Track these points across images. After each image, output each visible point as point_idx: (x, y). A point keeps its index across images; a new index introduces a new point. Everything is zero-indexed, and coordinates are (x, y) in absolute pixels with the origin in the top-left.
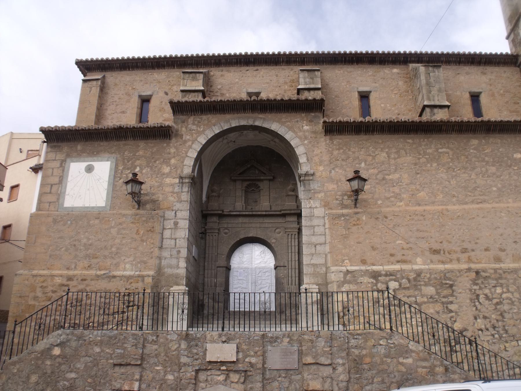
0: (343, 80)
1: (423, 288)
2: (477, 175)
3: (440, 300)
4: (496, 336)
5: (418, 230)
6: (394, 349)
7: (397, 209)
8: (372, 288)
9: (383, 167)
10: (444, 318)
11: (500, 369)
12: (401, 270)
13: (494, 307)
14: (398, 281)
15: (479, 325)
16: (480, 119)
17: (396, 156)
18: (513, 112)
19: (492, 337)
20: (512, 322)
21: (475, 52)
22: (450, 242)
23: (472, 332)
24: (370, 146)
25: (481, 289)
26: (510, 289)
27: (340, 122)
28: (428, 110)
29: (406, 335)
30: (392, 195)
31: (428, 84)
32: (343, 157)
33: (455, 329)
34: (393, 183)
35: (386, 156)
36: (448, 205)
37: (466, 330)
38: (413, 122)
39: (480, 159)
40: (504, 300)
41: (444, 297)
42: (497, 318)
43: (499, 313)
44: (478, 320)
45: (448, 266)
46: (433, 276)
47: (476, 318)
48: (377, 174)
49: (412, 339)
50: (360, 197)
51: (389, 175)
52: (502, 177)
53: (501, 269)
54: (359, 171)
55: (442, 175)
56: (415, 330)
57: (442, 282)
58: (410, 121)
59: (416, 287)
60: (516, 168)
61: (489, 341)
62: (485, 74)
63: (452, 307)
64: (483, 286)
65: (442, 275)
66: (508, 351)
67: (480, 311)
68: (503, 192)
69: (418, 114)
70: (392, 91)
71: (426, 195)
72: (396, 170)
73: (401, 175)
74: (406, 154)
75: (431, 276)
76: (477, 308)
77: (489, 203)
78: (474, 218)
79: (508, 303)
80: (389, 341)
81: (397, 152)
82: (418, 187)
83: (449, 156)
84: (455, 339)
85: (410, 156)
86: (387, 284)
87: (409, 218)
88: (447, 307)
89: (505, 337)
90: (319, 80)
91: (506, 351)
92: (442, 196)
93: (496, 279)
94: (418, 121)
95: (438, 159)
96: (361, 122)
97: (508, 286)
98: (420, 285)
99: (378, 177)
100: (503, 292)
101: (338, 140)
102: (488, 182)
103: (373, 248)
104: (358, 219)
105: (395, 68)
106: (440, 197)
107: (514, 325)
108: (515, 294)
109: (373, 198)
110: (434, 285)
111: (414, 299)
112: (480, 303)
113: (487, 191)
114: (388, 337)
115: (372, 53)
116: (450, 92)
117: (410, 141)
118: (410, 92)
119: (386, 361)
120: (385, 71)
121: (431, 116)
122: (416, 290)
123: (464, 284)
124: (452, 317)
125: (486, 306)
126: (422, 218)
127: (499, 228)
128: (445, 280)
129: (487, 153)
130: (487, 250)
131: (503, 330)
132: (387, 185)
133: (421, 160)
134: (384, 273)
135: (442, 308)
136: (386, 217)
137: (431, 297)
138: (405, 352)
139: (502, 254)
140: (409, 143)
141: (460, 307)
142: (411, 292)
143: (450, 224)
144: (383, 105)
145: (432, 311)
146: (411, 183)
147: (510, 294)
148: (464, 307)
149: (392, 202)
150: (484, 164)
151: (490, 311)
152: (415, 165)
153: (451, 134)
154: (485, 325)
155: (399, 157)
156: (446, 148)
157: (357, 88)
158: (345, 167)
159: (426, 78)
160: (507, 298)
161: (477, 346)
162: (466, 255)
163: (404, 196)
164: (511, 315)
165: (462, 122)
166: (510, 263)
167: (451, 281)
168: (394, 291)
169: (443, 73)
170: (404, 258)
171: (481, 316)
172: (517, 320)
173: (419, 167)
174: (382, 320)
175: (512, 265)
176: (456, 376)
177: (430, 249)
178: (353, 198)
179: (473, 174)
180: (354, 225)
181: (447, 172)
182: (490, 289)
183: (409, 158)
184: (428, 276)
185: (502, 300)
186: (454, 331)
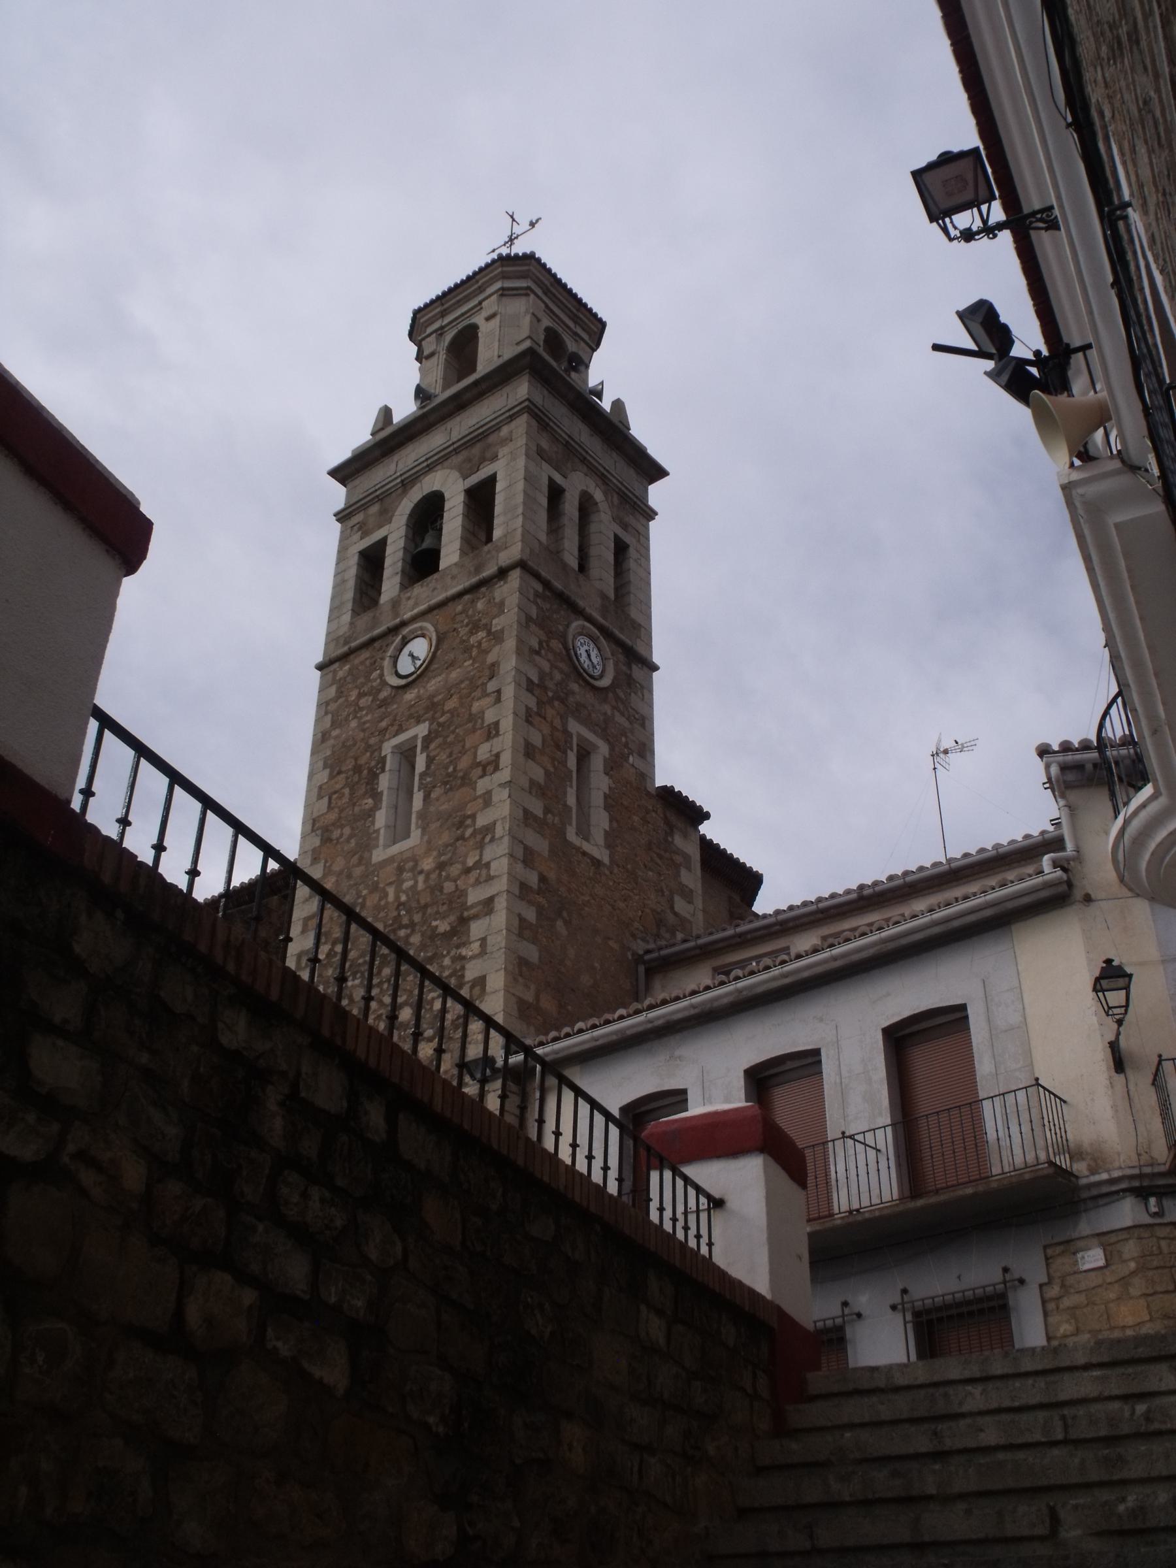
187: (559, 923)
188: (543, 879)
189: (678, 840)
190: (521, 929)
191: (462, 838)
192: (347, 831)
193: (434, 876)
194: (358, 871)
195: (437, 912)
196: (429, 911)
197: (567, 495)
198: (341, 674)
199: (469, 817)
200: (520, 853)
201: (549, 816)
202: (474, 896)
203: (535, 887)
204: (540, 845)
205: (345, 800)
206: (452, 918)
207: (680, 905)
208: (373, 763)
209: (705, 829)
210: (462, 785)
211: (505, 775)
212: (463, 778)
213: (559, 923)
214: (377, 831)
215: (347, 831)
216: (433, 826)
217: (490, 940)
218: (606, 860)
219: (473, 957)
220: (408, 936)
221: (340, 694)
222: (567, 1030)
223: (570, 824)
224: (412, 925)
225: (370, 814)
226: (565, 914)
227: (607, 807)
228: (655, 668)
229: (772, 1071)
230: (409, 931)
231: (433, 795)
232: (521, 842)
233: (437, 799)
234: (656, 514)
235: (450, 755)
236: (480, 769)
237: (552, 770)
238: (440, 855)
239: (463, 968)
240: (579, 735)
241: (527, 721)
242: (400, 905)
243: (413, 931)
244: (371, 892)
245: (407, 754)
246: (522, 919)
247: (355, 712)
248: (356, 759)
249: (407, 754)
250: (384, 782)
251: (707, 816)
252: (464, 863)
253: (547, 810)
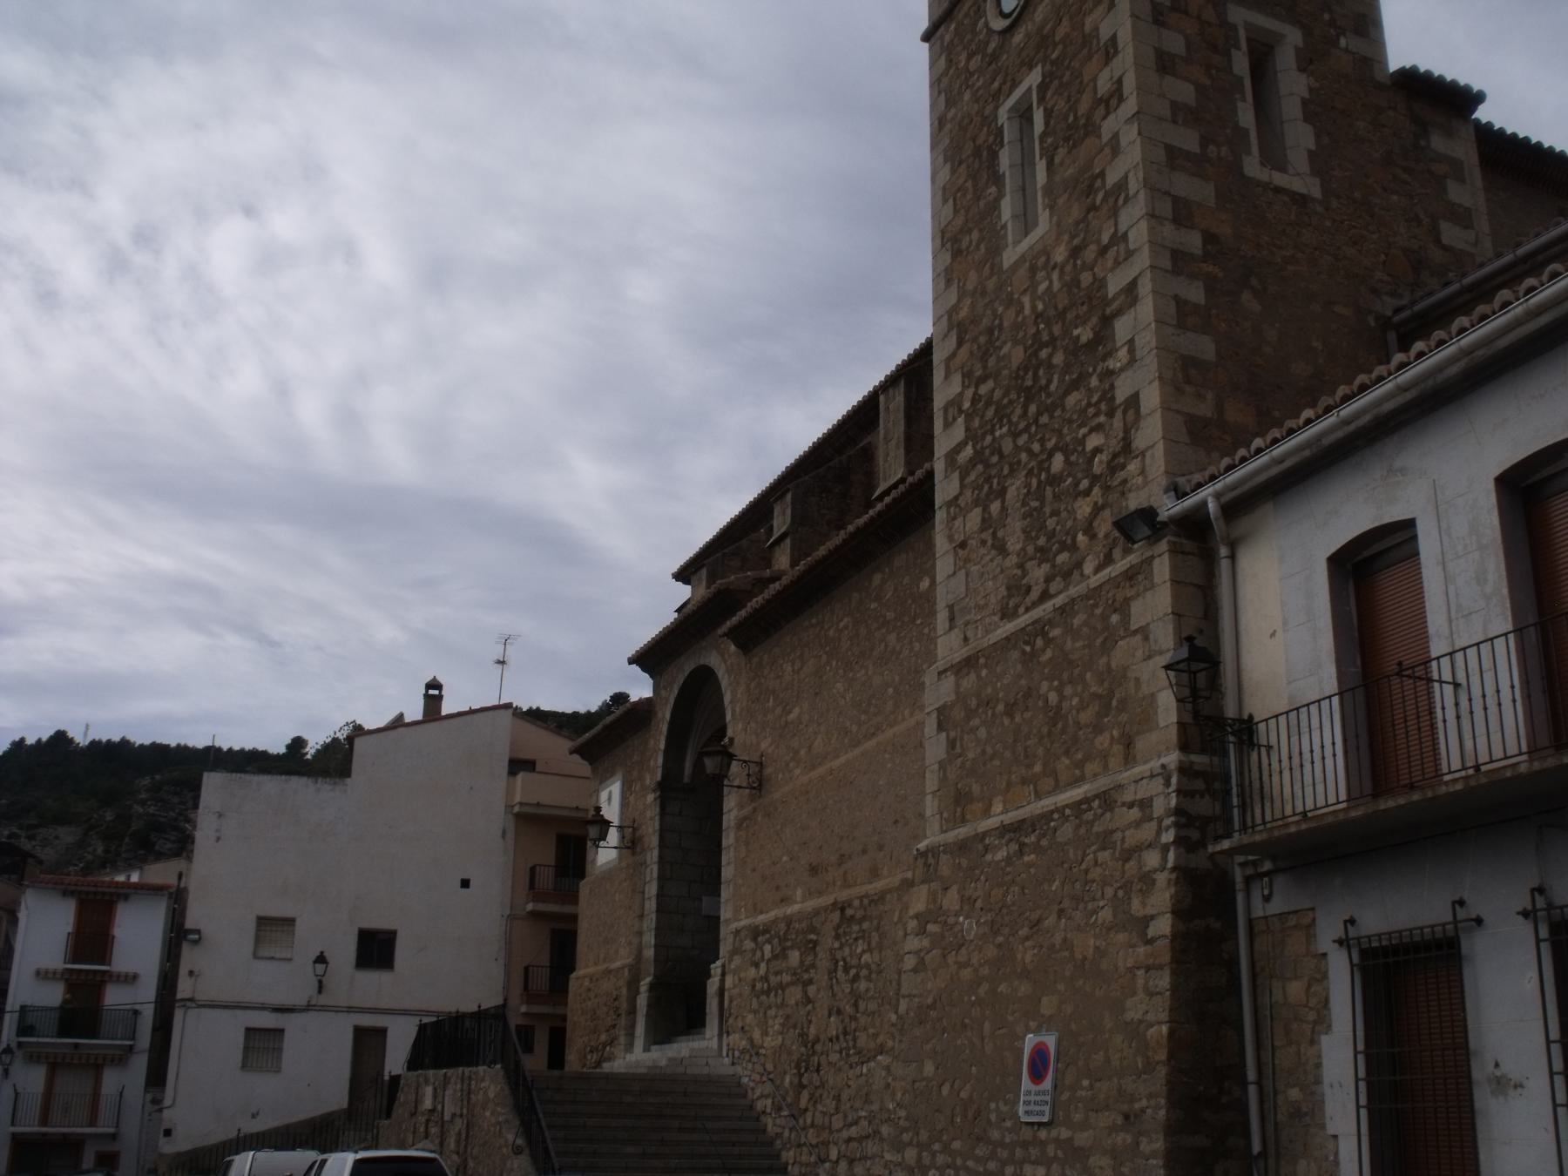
187: (1246, 296)
188: (1209, 238)
189: (1438, 143)
190: (1183, 316)
191: (1093, 208)
192: (975, 235)
193: (1068, 268)
194: (991, 284)
195: (1077, 317)
196: (1070, 316)
198: (947, 38)
199: (1097, 176)
200: (1166, 208)
201: (1212, 148)
202: (1115, 284)
203: (1199, 252)
204: (1200, 191)
205: (969, 196)
206: (1094, 320)
207: (1451, 234)
208: (991, 139)
209: (1483, 114)
210: (1086, 135)
211: (1130, 106)
212: (1085, 126)
213: (1246, 296)
214: (1004, 227)
215: (975, 235)
216: (1061, 201)
217: (1138, 343)
218: (1316, 192)
219: (1122, 370)
220: (1051, 356)
221: (950, 61)
222: (1242, 452)
223: (1249, 153)
224: (1053, 341)
225: (995, 206)
226: (1254, 282)
227: (1307, 119)
229: (1545, 473)
230: (1050, 350)
231: (1057, 160)
232: (1167, 193)
233: (1061, 164)
235: (1069, 100)
236: (1102, 107)
237: (1208, 82)
238: (1073, 237)
239: (1112, 387)
240: (1249, 27)
241: (1156, 22)
242: (1038, 316)
243: (1055, 348)
244: (1007, 308)
245: (1024, 115)
246: (1180, 302)
247: (967, 79)
248: (974, 139)
249: (1024, 115)
250: (1005, 160)
251: (1479, 98)
252: (1098, 241)
253: (1205, 141)
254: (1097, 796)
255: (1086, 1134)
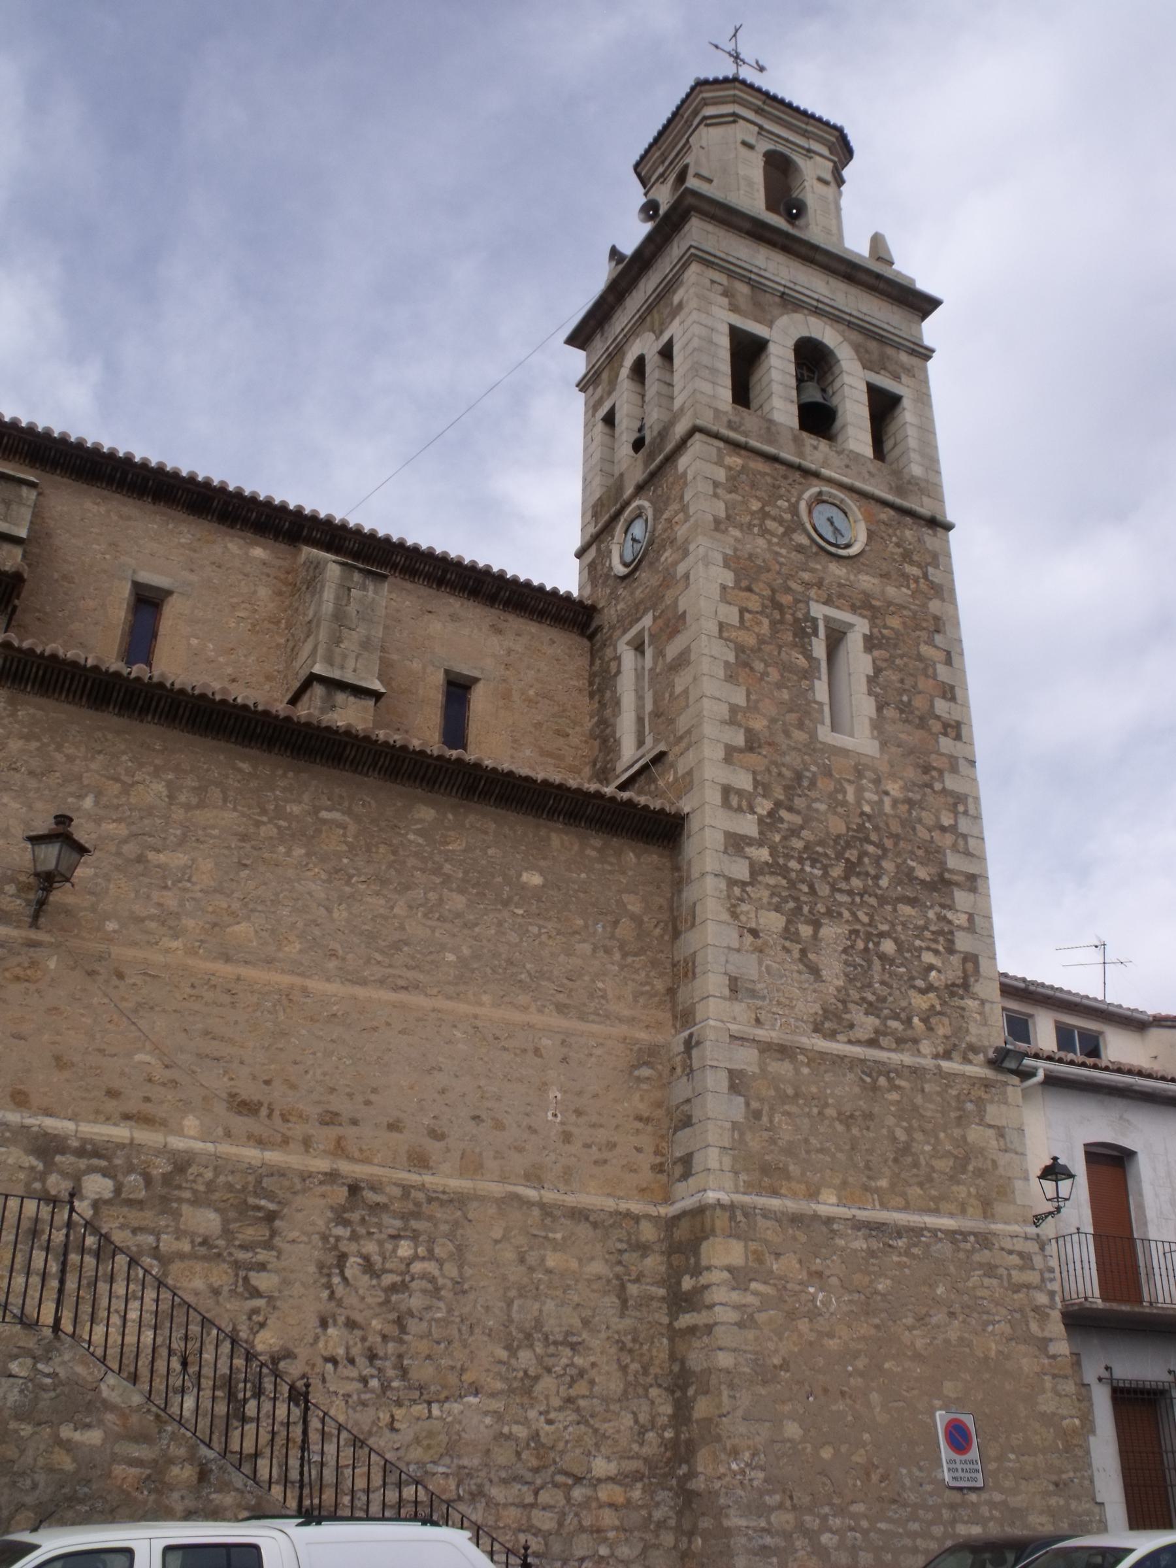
0: (101, 534)
1: (186, 1209)
2: (410, 907)
3: (230, 1254)
4: (374, 1383)
5: (206, 1033)
6: (52, 1394)
7: (160, 958)
8: (28, 1185)
9: (146, 822)
10: (231, 1311)
11: (361, 1484)
12: (132, 1143)
13: (382, 1297)
14: (113, 1177)
15: (331, 1344)
16: (454, 754)
17: (194, 801)
18: (549, 754)
19: (361, 1385)
20: (423, 1347)
21: (488, 566)
22: (293, 1087)
23: (307, 1363)
24: (124, 753)
25: (354, 1237)
26: (437, 1250)
27: (54, 657)
28: (318, 690)
29: (99, 1352)
30: (153, 911)
31: (339, 617)
32: (35, 763)
33: (260, 1347)
34: (164, 878)
35: (165, 793)
36: (309, 977)
37: (289, 1355)
38: (266, 713)
39: (430, 865)
40: (413, 1279)
41: (242, 1247)
42: (385, 1331)
43: (393, 1316)
44: (330, 1331)
45: (273, 1156)
46: (222, 1179)
47: (324, 1324)
48: (125, 841)
49: (116, 1367)
50: (56, 897)
51: (158, 851)
52: (477, 929)
53: (422, 1187)
54: (71, 820)
55: (312, 886)
56: (131, 1339)
57: (245, 1202)
58: (260, 708)
59: (165, 1205)
60: (520, 912)
61: (349, 1396)
62: (500, 632)
63: (262, 1281)
64: (362, 1231)
65: (251, 1178)
66: (397, 1431)
67: (340, 1303)
68: (473, 971)
69: (289, 696)
70: (234, 607)
71: (253, 934)
72: (182, 842)
73: (193, 860)
74: (225, 800)
75: (217, 1176)
76: (333, 1293)
77: (426, 995)
78: (375, 1029)
79: (424, 1291)
80: (40, 1366)
81: (201, 790)
82: (236, 905)
83: (344, 835)
84: (252, 1379)
85: (235, 809)
86: (77, 1178)
87: (189, 990)
88: (246, 1279)
89: (398, 1389)
90: (27, 514)
91: (393, 1429)
92: (298, 946)
93: (404, 1217)
94: (282, 714)
95: (313, 837)
96: (117, 674)
97: (432, 1241)
98: (180, 1200)
99: (126, 849)
100: (416, 1257)
101: (32, 711)
102: (437, 934)
103: (60, 1062)
104: (33, 964)
105: (257, 544)
106: (293, 949)
107: (429, 1357)
108: (447, 1266)
109: (93, 908)
110: (222, 1205)
111: (151, 1239)
112: (345, 1279)
113: (429, 958)
114: (38, 1353)
115: (207, 484)
116: (395, 657)
117: (245, 766)
118: (283, 625)
119: (16, 1431)
120: (230, 545)
121: (323, 711)
122: (163, 1213)
123: (309, 1215)
124: (255, 1311)
125: (361, 1292)
126: (226, 999)
127: (440, 1070)
128: (256, 1195)
129: (453, 851)
130: (394, 1127)
131: (394, 1368)
132: (147, 880)
133: (263, 829)
134: (75, 1144)
135: (232, 1280)
136: (120, 976)
137: (204, 1243)
138: (83, 1405)
139: (434, 1148)
140: (240, 770)
141: (286, 1282)
142: (147, 1217)
143: (304, 1032)
144: (194, 641)
145: (198, 1284)
146: (219, 890)
147: (433, 1263)
148: (297, 1284)
149: (147, 932)
150: (438, 881)
151: (369, 1307)
152: (243, 840)
153: (367, 775)
154: (348, 1348)
155: (201, 805)
156: (344, 813)
157: (134, 572)
158: (31, 794)
159: (337, 598)
160: (424, 1276)
161: (307, 1409)
162: (333, 1132)
163: (189, 923)
164: (425, 1325)
165: (404, 748)
166: (451, 1176)
167: (272, 1202)
168: (96, 1205)
169: (389, 598)
170: (147, 1108)
171: (341, 1320)
172: (438, 1343)
173: (253, 847)
174: (33, 1293)
175: (456, 1184)
176: (228, 1499)
177: (233, 1096)
178: (32, 896)
179: (401, 903)
180: (18, 978)
181: (329, 881)
182: (380, 1243)
183: (229, 816)
184: (209, 1175)
185: (408, 1278)
186: (250, 1356)
197: (772, 348)
228: (948, 527)
232: (719, 741)
234: (933, 351)
240: (827, 619)
254: (975, 1234)
255: (1019, 1498)
